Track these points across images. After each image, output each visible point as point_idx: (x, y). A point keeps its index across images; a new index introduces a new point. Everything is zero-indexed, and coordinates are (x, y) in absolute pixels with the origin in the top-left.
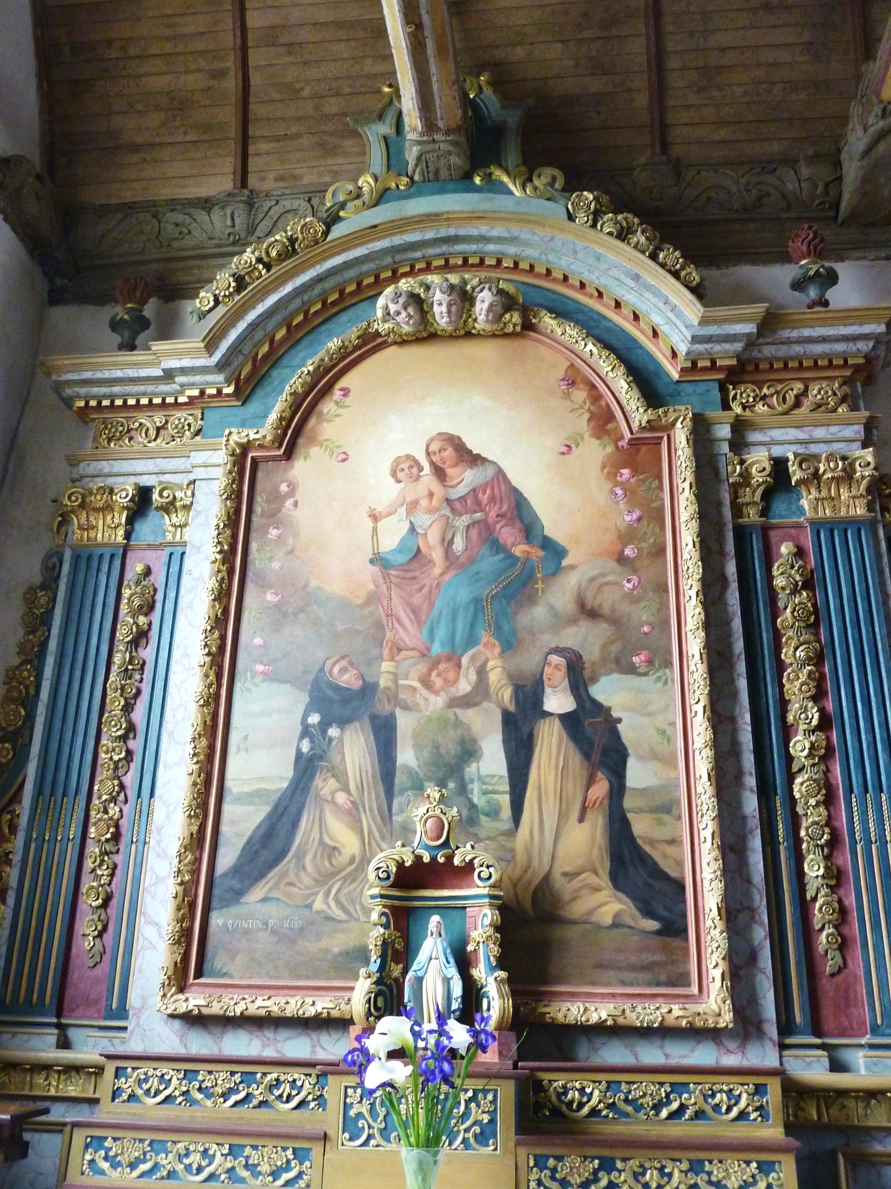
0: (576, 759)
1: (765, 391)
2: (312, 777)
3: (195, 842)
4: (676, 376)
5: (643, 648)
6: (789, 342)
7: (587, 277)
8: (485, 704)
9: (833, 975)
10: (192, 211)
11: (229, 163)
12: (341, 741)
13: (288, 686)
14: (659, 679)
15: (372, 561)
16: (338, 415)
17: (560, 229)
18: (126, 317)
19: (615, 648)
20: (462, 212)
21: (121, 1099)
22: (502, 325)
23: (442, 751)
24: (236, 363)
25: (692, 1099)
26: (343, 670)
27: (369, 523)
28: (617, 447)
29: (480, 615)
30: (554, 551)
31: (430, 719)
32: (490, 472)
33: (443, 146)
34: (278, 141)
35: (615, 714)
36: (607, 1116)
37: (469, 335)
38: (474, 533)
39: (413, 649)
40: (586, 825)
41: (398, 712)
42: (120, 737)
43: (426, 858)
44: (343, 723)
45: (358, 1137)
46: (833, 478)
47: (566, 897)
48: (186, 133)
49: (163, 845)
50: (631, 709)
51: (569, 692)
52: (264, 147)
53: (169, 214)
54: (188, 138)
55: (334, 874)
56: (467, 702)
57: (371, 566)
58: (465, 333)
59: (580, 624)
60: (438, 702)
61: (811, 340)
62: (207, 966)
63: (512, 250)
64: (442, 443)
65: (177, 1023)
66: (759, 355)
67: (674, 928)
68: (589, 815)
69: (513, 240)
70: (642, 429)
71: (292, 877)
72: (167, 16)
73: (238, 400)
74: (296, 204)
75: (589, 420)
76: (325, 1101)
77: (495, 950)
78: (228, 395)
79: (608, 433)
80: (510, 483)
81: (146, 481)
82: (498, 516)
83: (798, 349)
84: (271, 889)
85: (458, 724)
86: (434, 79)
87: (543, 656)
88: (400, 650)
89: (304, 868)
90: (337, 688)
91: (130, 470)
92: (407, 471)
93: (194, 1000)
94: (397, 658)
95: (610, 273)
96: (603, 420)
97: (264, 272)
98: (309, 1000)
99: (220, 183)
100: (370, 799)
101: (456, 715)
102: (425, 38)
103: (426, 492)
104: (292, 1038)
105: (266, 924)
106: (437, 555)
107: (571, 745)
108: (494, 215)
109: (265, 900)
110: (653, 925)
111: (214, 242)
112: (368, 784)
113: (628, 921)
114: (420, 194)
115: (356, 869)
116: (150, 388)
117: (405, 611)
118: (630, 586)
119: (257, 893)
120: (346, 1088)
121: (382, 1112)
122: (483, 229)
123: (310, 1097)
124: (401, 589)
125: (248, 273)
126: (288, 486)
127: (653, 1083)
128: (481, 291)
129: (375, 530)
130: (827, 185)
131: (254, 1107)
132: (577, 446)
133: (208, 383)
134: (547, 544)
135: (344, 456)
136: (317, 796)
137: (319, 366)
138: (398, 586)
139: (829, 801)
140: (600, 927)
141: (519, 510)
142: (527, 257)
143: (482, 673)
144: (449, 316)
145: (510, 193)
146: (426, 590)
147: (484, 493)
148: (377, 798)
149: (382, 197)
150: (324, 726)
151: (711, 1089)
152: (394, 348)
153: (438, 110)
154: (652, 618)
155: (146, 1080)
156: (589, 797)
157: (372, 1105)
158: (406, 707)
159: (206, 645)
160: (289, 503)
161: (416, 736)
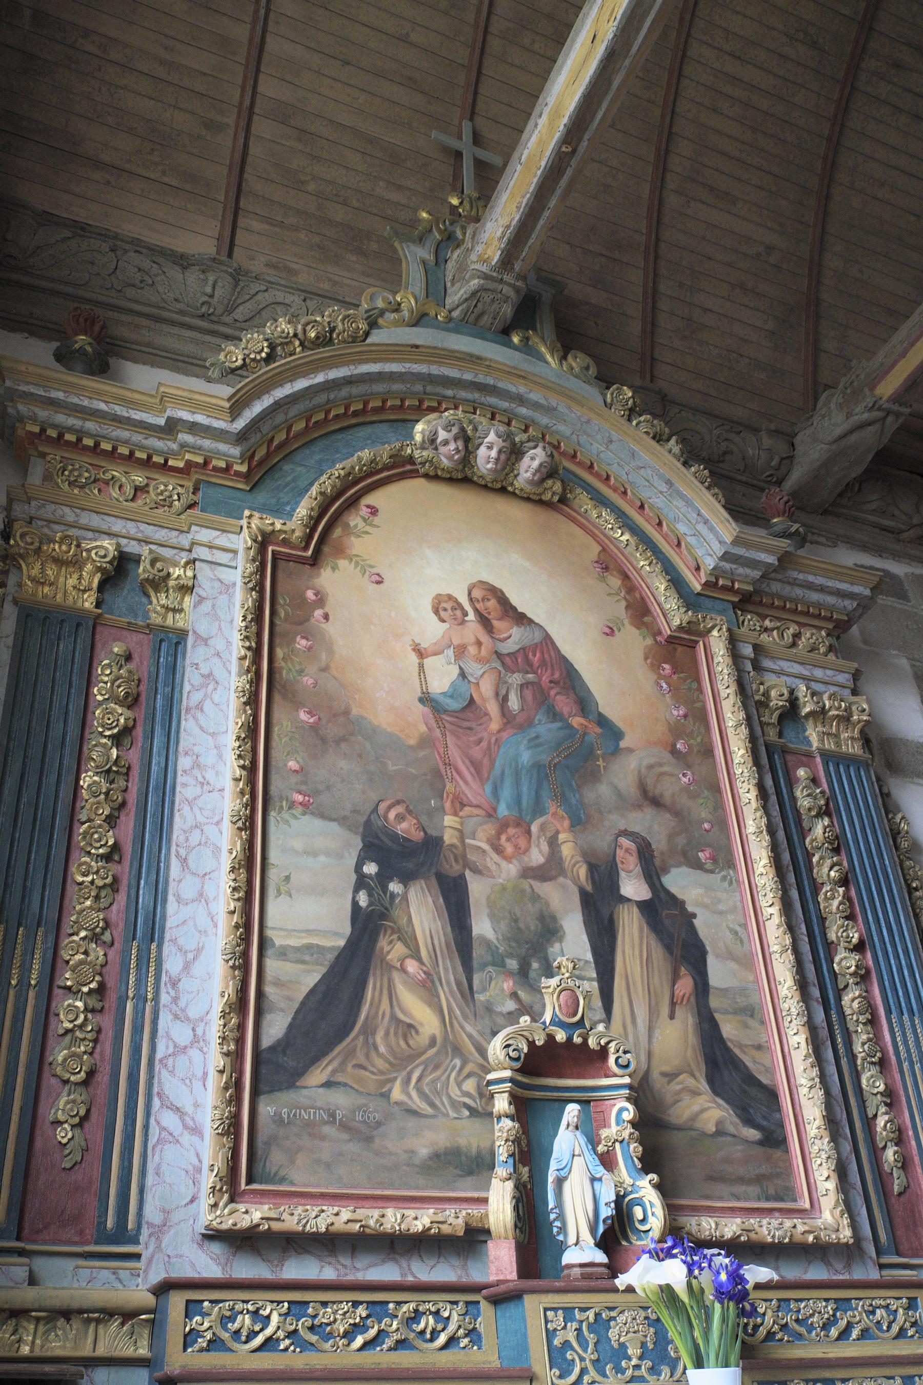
0: (658, 953)
1: (767, 623)
2: (374, 940)
3: (239, 1005)
4: (698, 588)
5: (709, 846)
6: (794, 583)
7: (614, 470)
8: (561, 879)
9: (900, 1194)
10: (161, 260)
11: (213, 227)
12: (405, 897)
13: (334, 825)
14: (724, 878)
15: (421, 700)
16: (367, 533)
17: (599, 415)
18: (89, 349)
19: (681, 841)
20: (505, 365)
21: (197, 1347)
22: (541, 490)
23: (522, 925)
24: (253, 440)
25: (857, 1314)
26: (400, 818)
27: (413, 658)
28: (656, 640)
29: (545, 782)
30: (612, 732)
31: (504, 888)
32: (538, 636)
33: (506, 290)
34: (271, 224)
35: (690, 908)
36: (781, 1340)
37: (503, 490)
38: (528, 693)
39: (477, 806)
40: (677, 1022)
41: (468, 874)
42: (102, 856)
43: (561, 1036)
44: (406, 879)
45: (569, 1372)
46: (838, 716)
47: (669, 1099)
48: (164, 173)
49: (182, 1003)
50: (705, 906)
51: (643, 880)
52: (256, 225)
53: (132, 254)
54: (166, 179)
55: (412, 1058)
56: (542, 874)
57: (421, 706)
58: (499, 487)
59: (645, 810)
60: (510, 870)
61: (810, 586)
62: (258, 1168)
63: (544, 420)
64: (484, 593)
65: (216, 1248)
66: (767, 590)
67: (774, 1139)
68: (679, 1011)
69: (549, 410)
70: (680, 628)
71: (361, 1059)
72: (166, 36)
73: (247, 483)
74: (289, 299)
75: (627, 608)
76: (479, 1336)
77: (635, 1148)
78: (237, 474)
79: (646, 625)
80: (559, 651)
81: (132, 547)
82: (551, 682)
83: (799, 592)
84: (334, 1072)
85: (535, 897)
86: (547, 213)
87: (613, 837)
88: (463, 805)
89: (376, 1048)
90: (395, 837)
91: (104, 527)
92: (450, 611)
93: (252, 1214)
94: (461, 814)
95: (642, 472)
96: (640, 611)
97: (298, 350)
98: (411, 1213)
99: (200, 241)
100: (446, 970)
101: (531, 887)
102: (569, 165)
103: (473, 640)
104: (376, 1265)
105: (333, 1115)
106: (493, 708)
107: (653, 936)
108: (535, 379)
109: (328, 1084)
110: (753, 1134)
111: (178, 306)
112: (441, 951)
113: (732, 1129)
114: (457, 331)
115: (438, 1053)
116: (137, 438)
117: (464, 762)
118: (685, 780)
119: (317, 1075)
120: (546, 1310)
121: (591, 1338)
122: (521, 388)
123: (461, 1332)
124: (458, 737)
125: (281, 344)
126: (316, 594)
127: (826, 1300)
128: (535, 447)
129: (421, 666)
130: (782, 459)
131: (390, 1349)
132: (619, 630)
133: (218, 452)
134: (602, 721)
135: (378, 578)
136: (383, 960)
137: (349, 474)
138: (453, 733)
139: (873, 1022)
140: (704, 1134)
141: (570, 678)
142: (557, 432)
143: (553, 842)
144: (496, 464)
145: (547, 362)
146: (484, 744)
147: (535, 655)
148: (454, 969)
149: (420, 319)
150: (383, 878)
151: (871, 1305)
152: (421, 482)
153: (527, 248)
154: (710, 816)
155: (232, 1319)
156: (676, 993)
157: (579, 1330)
158: (476, 871)
159: (240, 756)
160: (318, 613)
161: (491, 904)
